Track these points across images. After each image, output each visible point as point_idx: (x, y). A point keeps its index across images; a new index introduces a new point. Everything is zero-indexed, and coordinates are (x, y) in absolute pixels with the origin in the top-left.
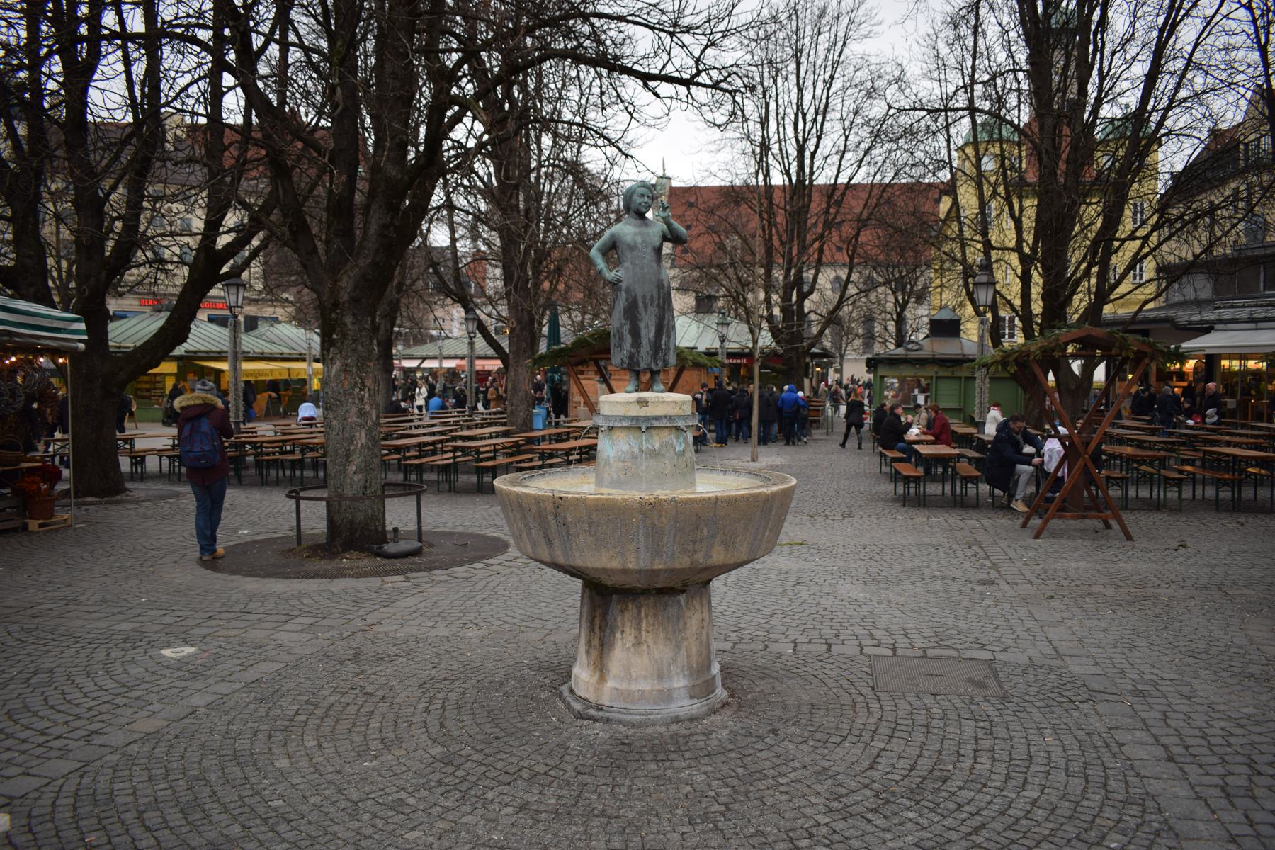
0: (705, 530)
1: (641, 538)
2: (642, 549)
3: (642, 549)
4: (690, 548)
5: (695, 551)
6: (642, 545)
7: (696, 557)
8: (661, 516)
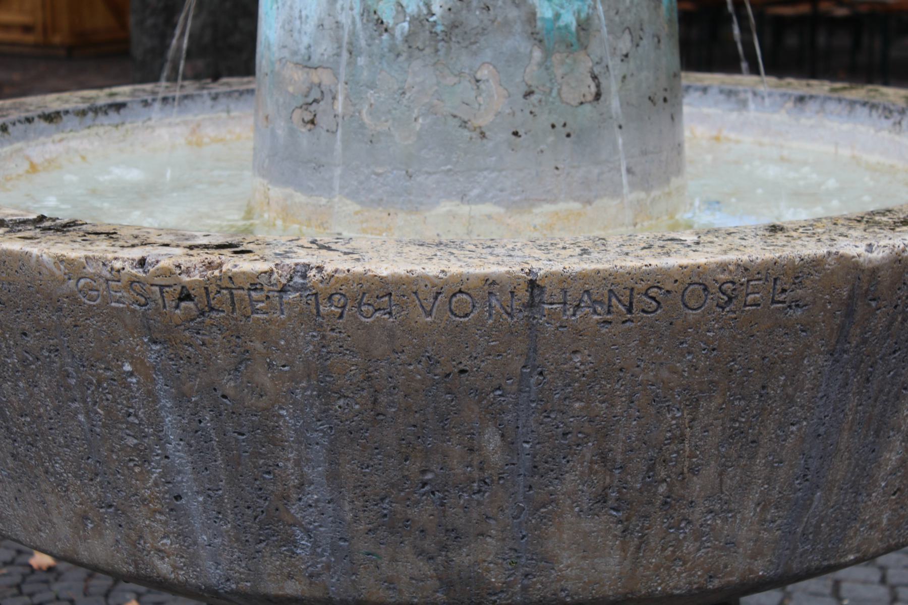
0: (491, 441)
1: (179, 454)
2: (195, 503)
3: (195, 503)
4: (424, 513)
5: (455, 535)
6: (187, 482)
7: (462, 558)
8: (244, 358)
